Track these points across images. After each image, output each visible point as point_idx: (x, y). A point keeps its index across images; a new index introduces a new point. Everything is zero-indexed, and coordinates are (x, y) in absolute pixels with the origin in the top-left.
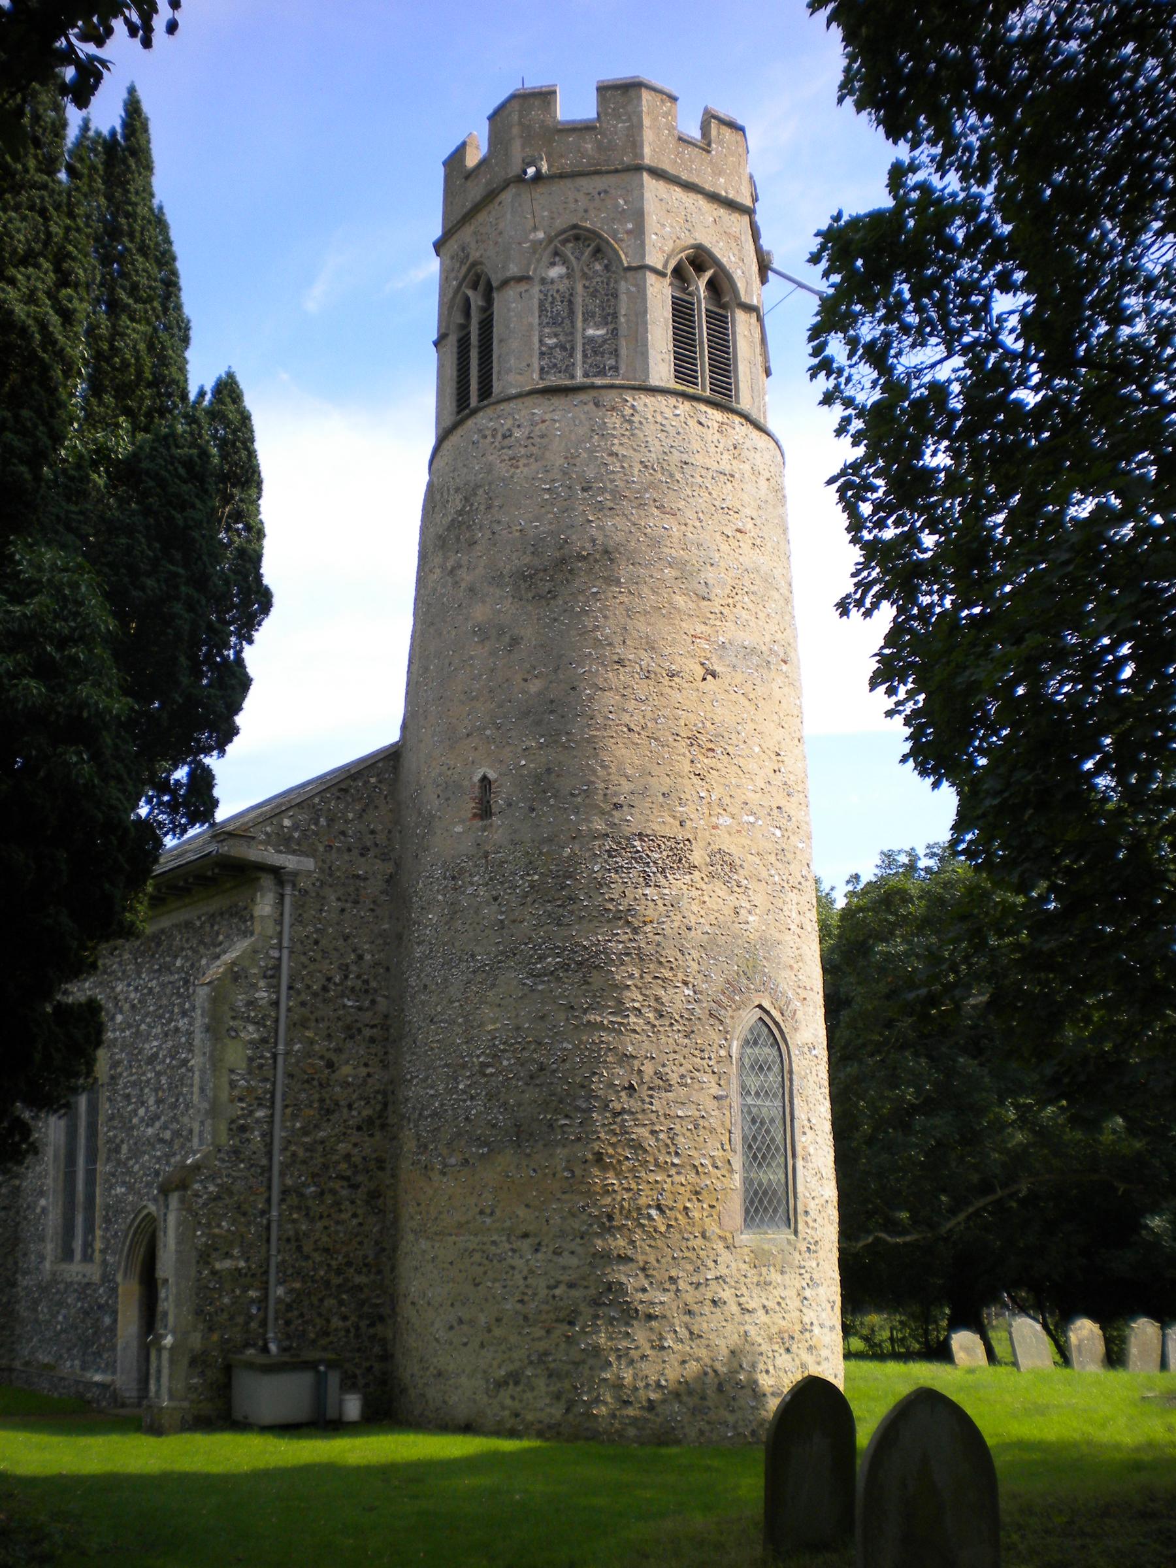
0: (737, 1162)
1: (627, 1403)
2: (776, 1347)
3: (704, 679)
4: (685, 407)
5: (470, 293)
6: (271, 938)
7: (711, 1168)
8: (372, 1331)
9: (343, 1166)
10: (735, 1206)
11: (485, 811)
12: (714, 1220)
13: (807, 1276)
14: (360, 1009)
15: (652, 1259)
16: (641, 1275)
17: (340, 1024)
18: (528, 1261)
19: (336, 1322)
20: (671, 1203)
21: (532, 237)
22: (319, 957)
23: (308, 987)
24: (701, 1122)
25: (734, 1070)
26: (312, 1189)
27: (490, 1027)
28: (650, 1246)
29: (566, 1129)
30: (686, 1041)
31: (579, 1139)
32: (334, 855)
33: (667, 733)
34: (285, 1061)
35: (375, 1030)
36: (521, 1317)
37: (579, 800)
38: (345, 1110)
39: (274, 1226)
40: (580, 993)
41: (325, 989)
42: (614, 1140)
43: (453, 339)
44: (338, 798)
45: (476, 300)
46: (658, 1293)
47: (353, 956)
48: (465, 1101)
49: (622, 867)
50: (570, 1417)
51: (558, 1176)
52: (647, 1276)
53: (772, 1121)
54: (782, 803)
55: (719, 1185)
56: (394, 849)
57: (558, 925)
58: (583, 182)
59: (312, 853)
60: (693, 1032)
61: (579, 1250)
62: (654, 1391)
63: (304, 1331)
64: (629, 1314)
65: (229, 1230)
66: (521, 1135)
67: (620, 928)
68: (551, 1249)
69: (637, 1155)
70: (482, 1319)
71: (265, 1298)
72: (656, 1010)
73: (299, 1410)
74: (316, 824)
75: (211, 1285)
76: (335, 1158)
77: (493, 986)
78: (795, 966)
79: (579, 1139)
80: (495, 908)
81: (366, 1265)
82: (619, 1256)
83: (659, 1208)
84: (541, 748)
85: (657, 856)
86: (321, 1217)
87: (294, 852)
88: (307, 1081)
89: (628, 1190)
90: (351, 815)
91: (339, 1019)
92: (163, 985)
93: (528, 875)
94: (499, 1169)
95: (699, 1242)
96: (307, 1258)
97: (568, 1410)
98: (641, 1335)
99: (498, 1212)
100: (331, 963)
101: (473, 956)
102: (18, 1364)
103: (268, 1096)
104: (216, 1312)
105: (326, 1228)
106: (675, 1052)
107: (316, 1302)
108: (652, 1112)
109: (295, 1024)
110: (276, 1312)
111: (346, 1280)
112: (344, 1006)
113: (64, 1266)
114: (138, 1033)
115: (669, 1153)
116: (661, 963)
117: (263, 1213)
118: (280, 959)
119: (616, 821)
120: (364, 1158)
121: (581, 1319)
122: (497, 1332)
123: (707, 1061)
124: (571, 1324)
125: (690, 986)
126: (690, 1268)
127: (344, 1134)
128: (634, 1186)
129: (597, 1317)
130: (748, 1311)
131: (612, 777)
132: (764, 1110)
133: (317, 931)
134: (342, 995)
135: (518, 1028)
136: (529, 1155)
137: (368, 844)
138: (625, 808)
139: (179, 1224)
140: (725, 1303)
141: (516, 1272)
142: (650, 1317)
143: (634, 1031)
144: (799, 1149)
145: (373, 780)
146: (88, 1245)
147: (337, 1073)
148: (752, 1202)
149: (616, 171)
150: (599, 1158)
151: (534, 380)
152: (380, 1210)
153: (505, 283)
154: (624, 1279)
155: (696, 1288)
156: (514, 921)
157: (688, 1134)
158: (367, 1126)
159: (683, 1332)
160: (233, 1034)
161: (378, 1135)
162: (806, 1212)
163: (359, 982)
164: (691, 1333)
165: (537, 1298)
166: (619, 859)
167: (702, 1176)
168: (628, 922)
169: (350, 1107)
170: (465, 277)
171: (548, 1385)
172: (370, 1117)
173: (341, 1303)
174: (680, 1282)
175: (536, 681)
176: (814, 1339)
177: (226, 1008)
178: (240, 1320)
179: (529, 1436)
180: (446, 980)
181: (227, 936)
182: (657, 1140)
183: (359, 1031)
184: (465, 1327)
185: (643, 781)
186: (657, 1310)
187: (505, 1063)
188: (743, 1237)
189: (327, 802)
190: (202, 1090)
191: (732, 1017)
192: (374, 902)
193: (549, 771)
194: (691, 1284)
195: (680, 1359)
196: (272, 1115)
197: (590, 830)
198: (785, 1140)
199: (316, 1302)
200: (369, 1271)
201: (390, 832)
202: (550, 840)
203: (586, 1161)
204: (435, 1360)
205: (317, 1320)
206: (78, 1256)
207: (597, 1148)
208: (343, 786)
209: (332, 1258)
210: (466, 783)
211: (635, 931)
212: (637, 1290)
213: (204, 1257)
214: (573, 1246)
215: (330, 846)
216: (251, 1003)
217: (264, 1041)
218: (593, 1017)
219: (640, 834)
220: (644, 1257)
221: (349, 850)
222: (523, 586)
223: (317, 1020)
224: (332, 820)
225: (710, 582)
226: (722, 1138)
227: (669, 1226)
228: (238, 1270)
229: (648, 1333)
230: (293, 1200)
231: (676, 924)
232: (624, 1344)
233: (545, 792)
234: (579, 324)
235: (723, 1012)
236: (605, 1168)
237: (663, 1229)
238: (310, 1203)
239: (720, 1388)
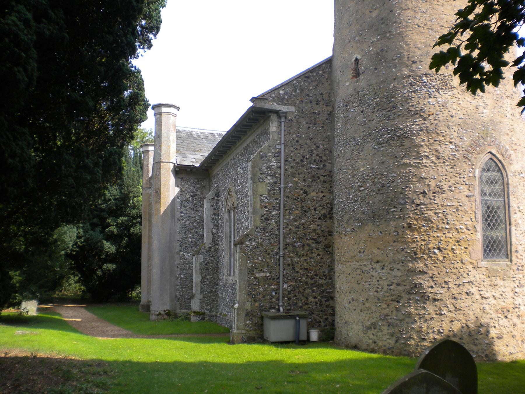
0: (479, 227)
1: (424, 339)
2: (499, 315)
6: (277, 140)
7: (465, 230)
8: (327, 303)
9: (313, 234)
10: (478, 248)
11: (357, 75)
12: (467, 255)
13: (517, 282)
14: (318, 169)
15: (436, 273)
16: (431, 280)
17: (309, 175)
18: (379, 273)
19: (311, 299)
20: (445, 247)
22: (298, 147)
23: (295, 160)
24: (460, 208)
25: (477, 182)
26: (299, 244)
27: (362, 169)
28: (435, 267)
29: (394, 213)
30: (452, 170)
31: (400, 217)
32: (304, 104)
33: (438, 26)
34: (284, 191)
35: (325, 177)
36: (377, 299)
37: (396, 61)
38: (313, 211)
39: (281, 259)
40: (399, 150)
41: (302, 161)
42: (417, 217)
44: (305, 81)
46: (439, 289)
47: (314, 147)
48: (352, 203)
49: (417, 90)
50: (398, 344)
52: (434, 281)
53: (498, 208)
55: (469, 238)
57: (389, 120)
59: (294, 105)
60: (455, 165)
61: (401, 268)
62: (437, 334)
63: (296, 303)
64: (425, 298)
65: (262, 261)
66: (375, 217)
67: (418, 118)
68: (389, 267)
69: (428, 224)
70: (361, 299)
71: (277, 290)
72: (436, 156)
73: (288, 336)
74: (295, 92)
75: (254, 283)
76: (309, 231)
77: (362, 151)
78: (510, 134)
79: (400, 217)
80: (362, 116)
81: (324, 275)
82: (420, 271)
83: (439, 249)
84: (378, 41)
85: (435, 83)
86: (303, 255)
87: (285, 104)
88: (295, 199)
89: (424, 240)
90: (311, 88)
91: (309, 173)
93: (375, 99)
94: (366, 232)
95: (460, 265)
96: (298, 272)
97: (397, 341)
98: (431, 308)
100: (304, 150)
101: (354, 139)
103: (278, 206)
104: (257, 294)
105: (305, 260)
106: (446, 175)
107: (302, 291)
108: (435, 204)
109: (289, 176)
110: (283, 294)
111: (316, 282)
112: (311, 168)
115: (443, 223)
116: (438, 133)
117: (277, 254)
118: (281, 149)
119: (414, 69)
120: (322, 231)
121: (403, 300)
122: (367, 305)
123: (462, 179)
124: (398, 302)
125: (453, 143)
126: (455, 277)
127: (313, 221)
128: (426, 238)
129: (410, 299)
130: (485, 298)
131: (411, 49)
132: (494, 202)
133: (298, 136)
135: (373, 169)
136: (378, 225)
137: (320, 99)
138: (418, 63)
140: (473, 294)
141: (374, 278)
142: (435, 300)
143: (426, 166)
144: (513, 221)
145: (320, 72)
147: (309, 195)
148: (488, 246)
150: (410, 226)
152: (330, 253)
154: (422, 282)
155: (458, 287)
156: (369, 121)
157: (453, 214)
159: (451, 308)
160: (261, 180)
162: (517, 251)
163: (318, 157)
164: (456, 308)
165: (383, 290)
166: (416, 87)
167: (461, 234)
168: (421, 116)
169: (315, 209)
171: (388, 330)
172: (325, 214)
173: (313, 291)
174: (450, 283)
175: (375, 11)
176: (521, 312)
177: (257, 170)
178: (268, 297)
179: (379, 353)
180: (344, 151)
182: (438, 217)
183: (319, 178)
184: (354, 302)
185: (426, 49)
186: (438, 297)
187: (368, 185)
188: (483, 263)
189: (300, 83)
191: (475, 158)
192: (323, 123)
193: (382, 50)
194: (455, 284)
195: (450, 320)
196: (280, 214)
197: (402, 75)
198: (505, 216)
199: (302, 291)
200: (326, 278)
201: (329, 94)
202: (384, 82)
203: (404, 227)
204: (344, 316)
205: (303, 298)
207: (409, 221)
208: (307, 75)
209: (309, 272)
210: (349, 63)
211: (425, 119)
212: (429, 287)
213: (251, 272)
214: (399, 266)
215: (302, 101)
216: (268, 168)
217: (275, 183)
218: (406, 161)
219: (426, 74)
220: (432, 272)
221: (311, 102)
223: (299, 174)
224: (302, 90)
226: (471, 215)
227: (444, 257)
228: (267, 277)
229: (434, 307)
230: (290, 248)
231: (445, 115)
232: (423, 312)
233: (381, 60)
235: (470, 155)
236: (413, 230)
237: (441, 259)
238: (298, 249)
239: (470, 335)
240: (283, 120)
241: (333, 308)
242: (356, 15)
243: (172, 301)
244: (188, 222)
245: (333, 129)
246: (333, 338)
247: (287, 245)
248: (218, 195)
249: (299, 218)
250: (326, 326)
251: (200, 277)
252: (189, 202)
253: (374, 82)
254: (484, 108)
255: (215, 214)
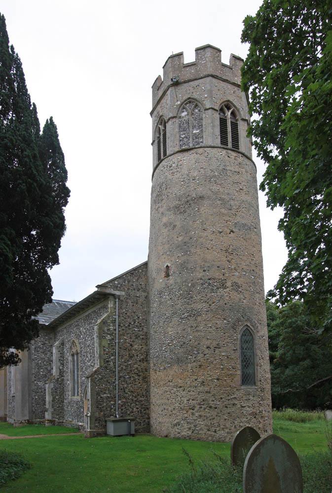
3: (230, 233)
4: (224, 152)
5: (160, 126)
8: (145, 412)
9: (136, 370)
11: (167, 275)
14: (139, 331)
21: (176, 104)
27: (170, 333)
34: (118, 344)
41: (129, 326)
43: (156, 142)
45: (162, 127)
47: (137, 317)
51: (189, 371)
54: (254, 269)
56: (147, 289)
58: (191, 83)
59: (124, 290)
70: (170, 409)
71: (114, 405)
91: (133, 333)
92: (90, 327)
97: (193, 432)
99: (173, 381)
102: (64, 421)
110: (118, 407)
113: (74, 397)
114: (86, 340)
122: (173, 412)
134: (134, 328)
139: (91, 385)
146: (78, 392)
149: (202, 78)
151: (177, 149)
153: (169, 119)
158: (142, 361)
161: (145, 363)
169: (137, 356)
170: (158, 122)
173: (136, 405)
178: (109, 409)
181: (103, 313)
183: (139, 336)
190: (97, 352)
193: (185, 262)
202: (185, 282)
206: (76, 395)
208: (132, 272)
217: (113, 339)
221: (134, 290)
222: (176, 210)
225: (232, 205)
228: (108, 397)
234: (191, 130)
240: (117, 300)
241: (148, 415)
242: (168, 238)
243: (29, 413)
244: (40, 362)
245: (149, 307)
246: (149, 432)
247: (121, 377)
248: (63, 344)
249: (128, 361)
250: (144, 425)
251: (52, 398)
252: (40, 348)
253: (179, 281)
254: (244, 299)
255: (61, 357)
